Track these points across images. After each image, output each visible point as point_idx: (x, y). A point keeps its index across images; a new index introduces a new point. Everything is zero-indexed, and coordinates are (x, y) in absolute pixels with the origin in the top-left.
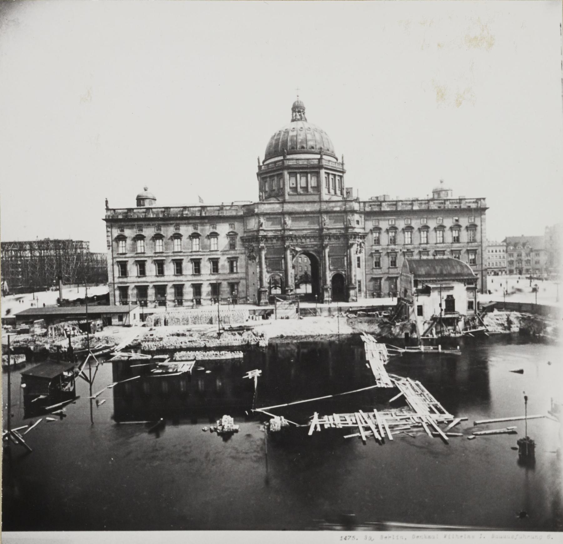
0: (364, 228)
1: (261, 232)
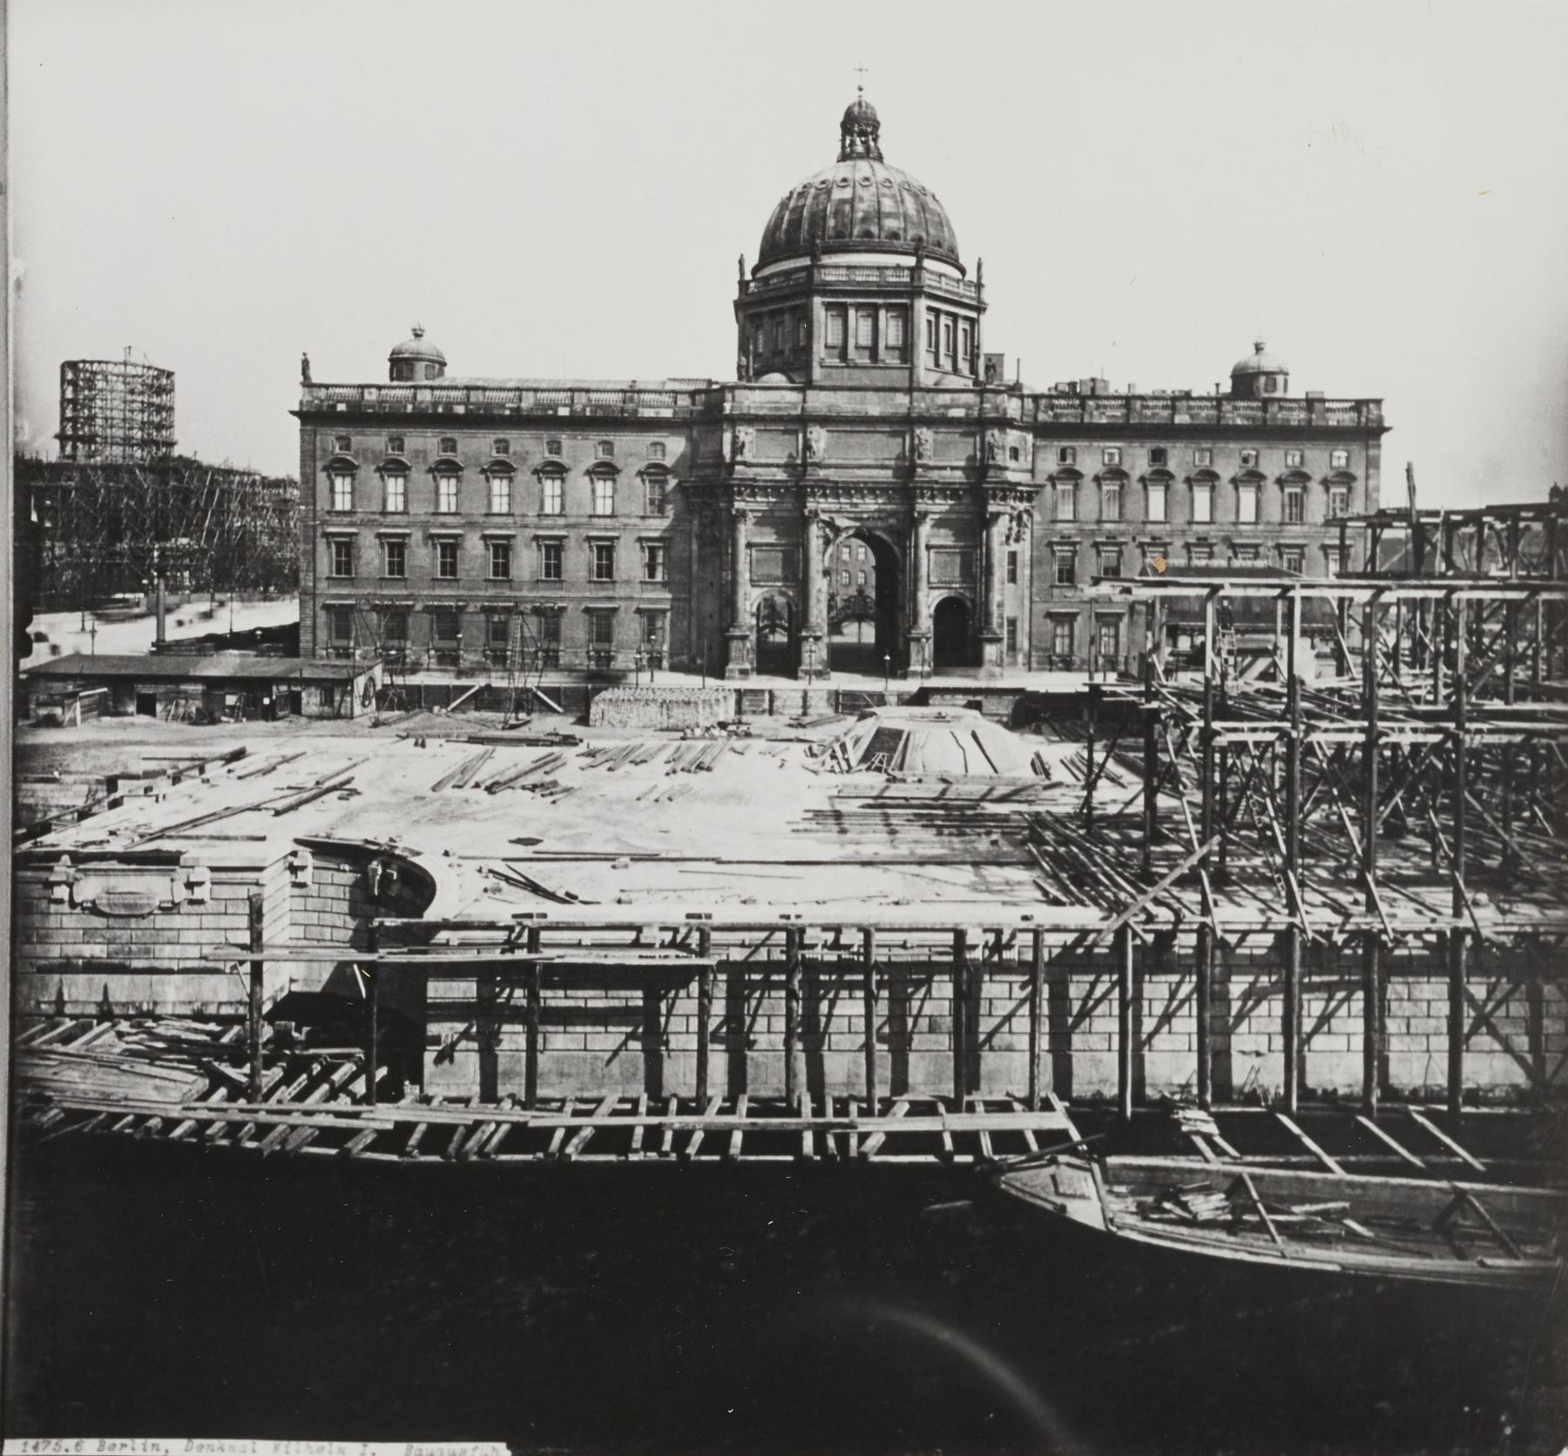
0: (1032, 471)
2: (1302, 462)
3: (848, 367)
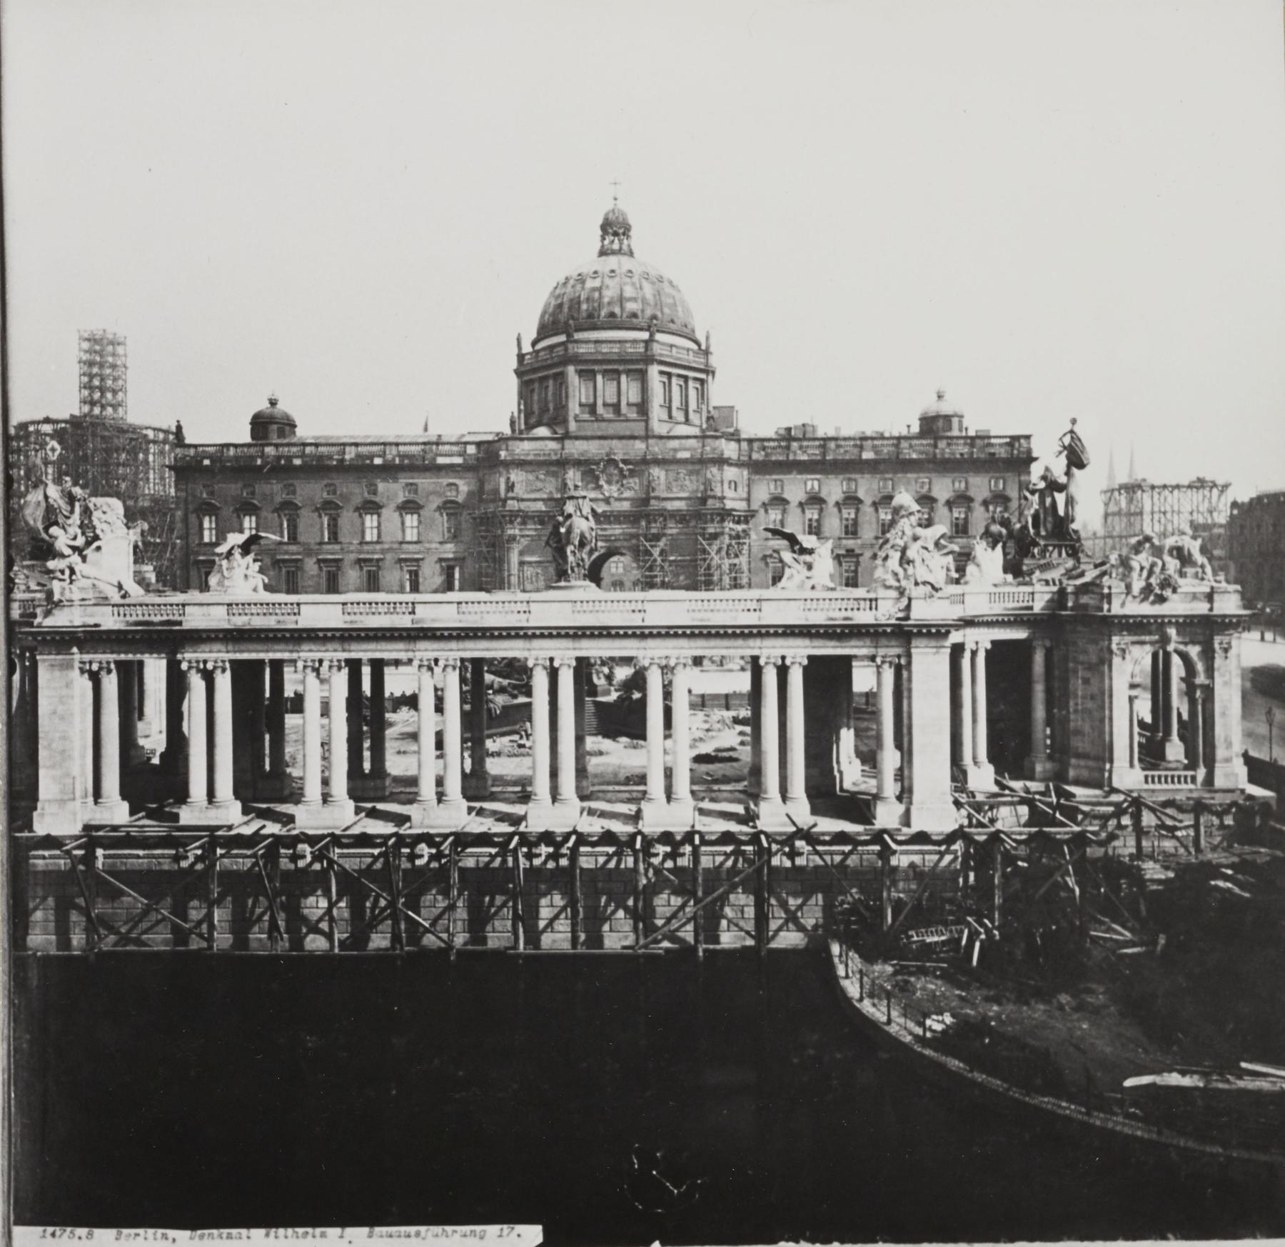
0: (748, 500)
1: (509, 502)
2: (967, 487)
3: (597, 420)
